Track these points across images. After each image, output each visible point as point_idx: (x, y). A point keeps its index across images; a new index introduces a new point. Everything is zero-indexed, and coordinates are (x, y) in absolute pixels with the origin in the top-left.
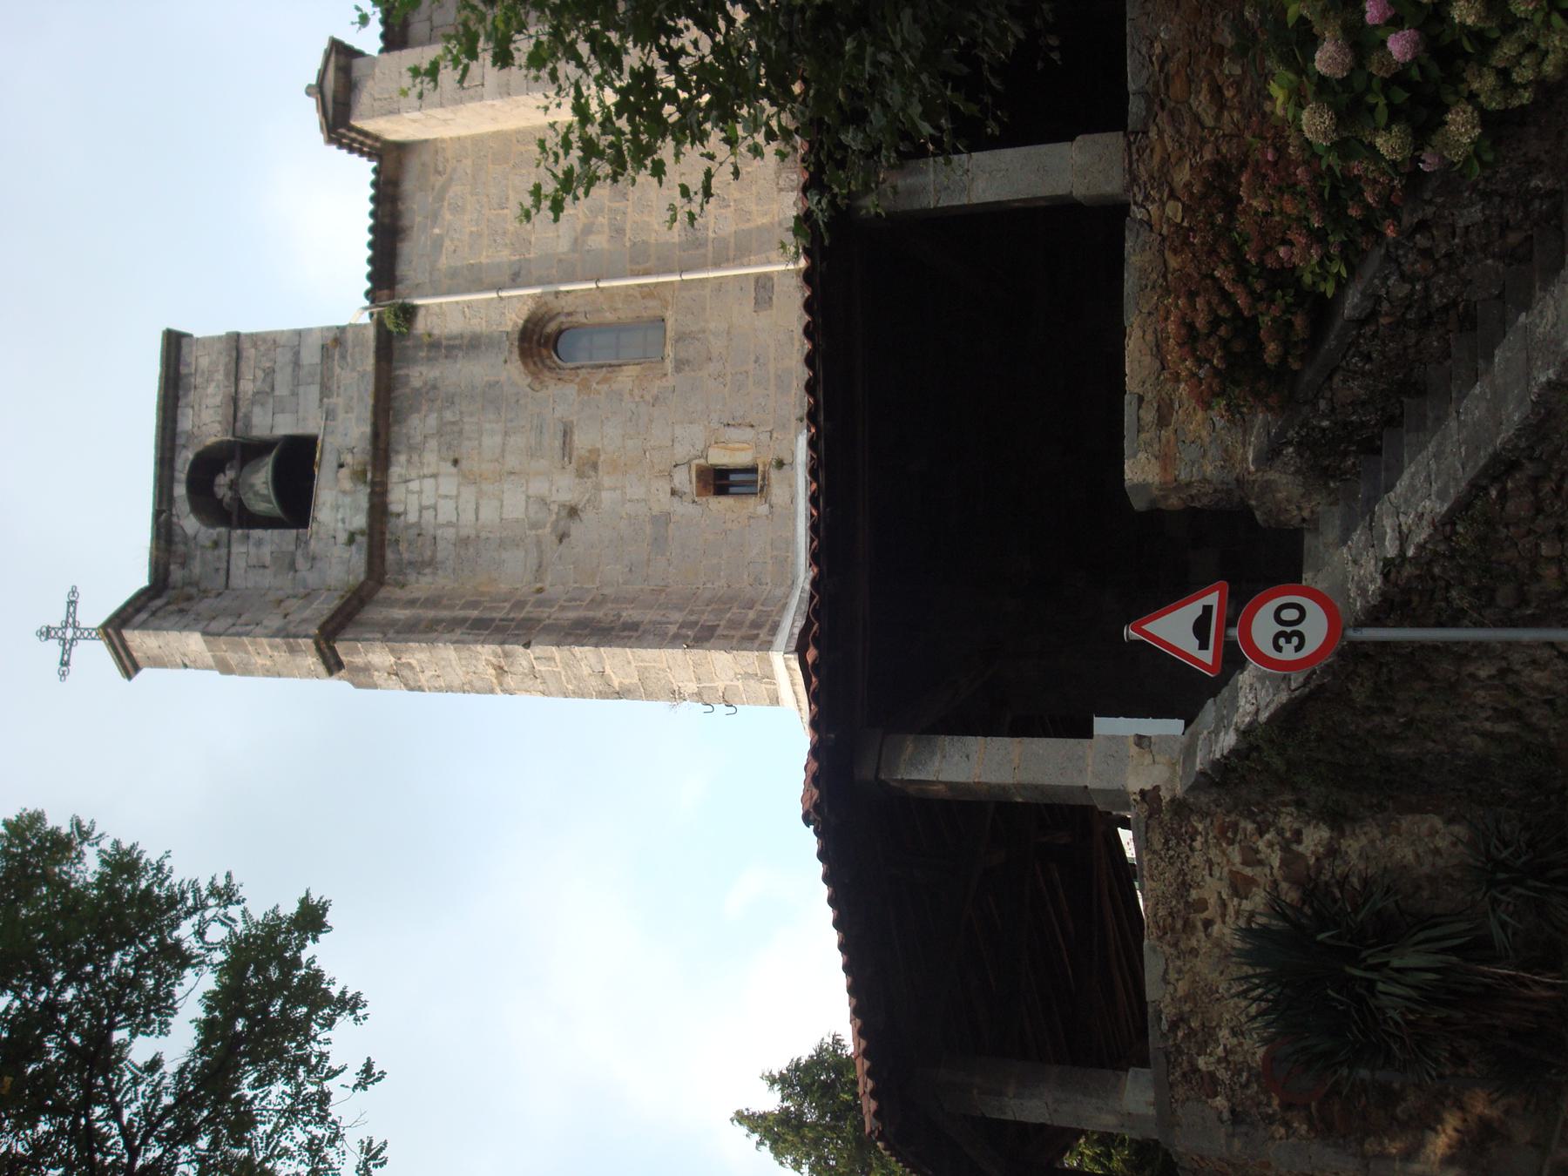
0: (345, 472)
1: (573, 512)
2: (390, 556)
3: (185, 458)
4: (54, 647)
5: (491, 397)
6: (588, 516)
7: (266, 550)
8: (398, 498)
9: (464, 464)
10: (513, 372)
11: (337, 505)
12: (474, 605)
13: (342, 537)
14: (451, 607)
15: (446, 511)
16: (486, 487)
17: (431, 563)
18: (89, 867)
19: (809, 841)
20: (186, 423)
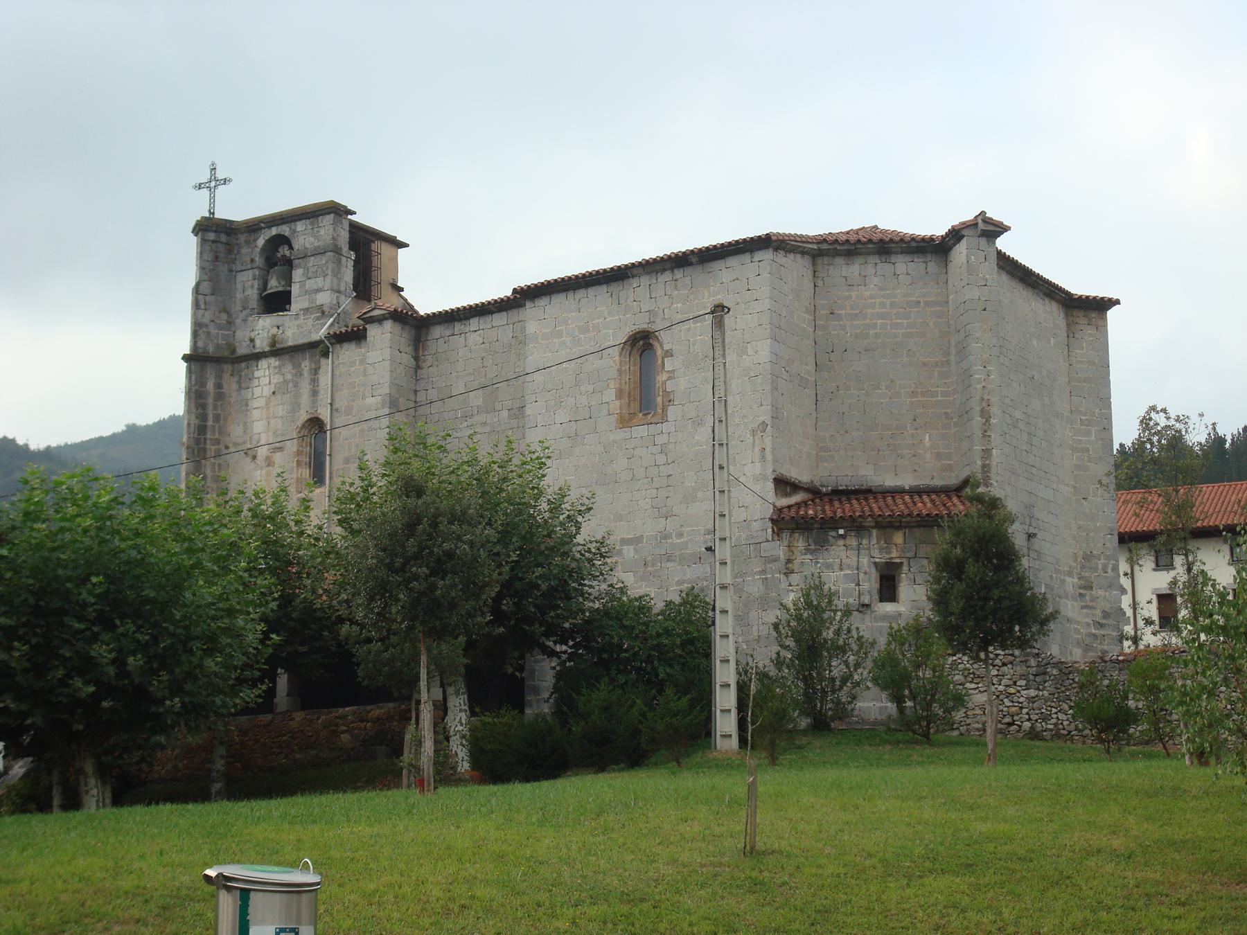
0: (275, 330)
1: (254, 457)
2: (243, 365)
3: (285, 230)
4: (220, 176)
5: (295, 406)
6: (253, 465)
7: (249, 292)
8: (263, 363)
9: (273, 398)
10: (303, 417)
11: (263, 328)
12: (217, 418)
13: (253, 335)
14: (215, 408)
15: (257, 392)
16: (264, 412)
17: (241, 388)
18: (93, 791)
19: (119, 428)
20: (300, 226)
